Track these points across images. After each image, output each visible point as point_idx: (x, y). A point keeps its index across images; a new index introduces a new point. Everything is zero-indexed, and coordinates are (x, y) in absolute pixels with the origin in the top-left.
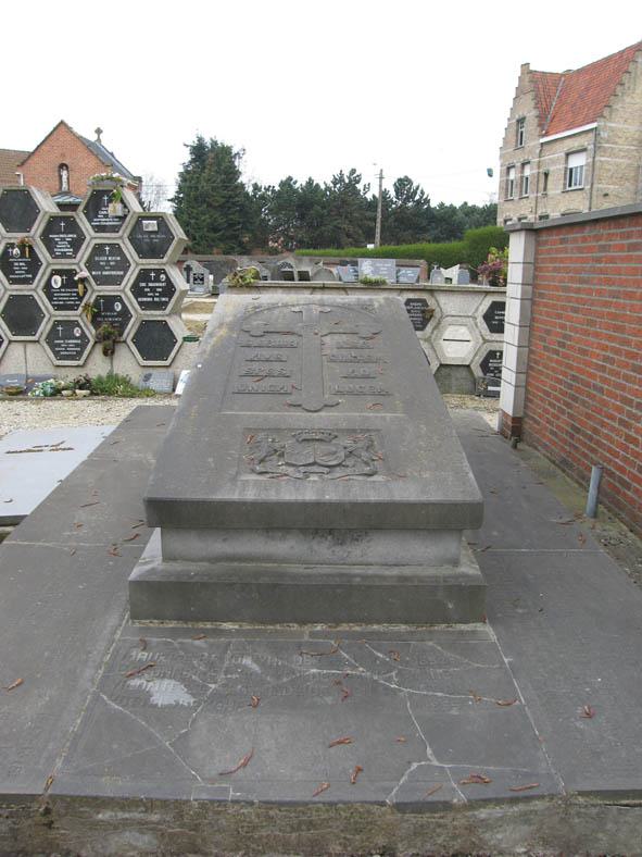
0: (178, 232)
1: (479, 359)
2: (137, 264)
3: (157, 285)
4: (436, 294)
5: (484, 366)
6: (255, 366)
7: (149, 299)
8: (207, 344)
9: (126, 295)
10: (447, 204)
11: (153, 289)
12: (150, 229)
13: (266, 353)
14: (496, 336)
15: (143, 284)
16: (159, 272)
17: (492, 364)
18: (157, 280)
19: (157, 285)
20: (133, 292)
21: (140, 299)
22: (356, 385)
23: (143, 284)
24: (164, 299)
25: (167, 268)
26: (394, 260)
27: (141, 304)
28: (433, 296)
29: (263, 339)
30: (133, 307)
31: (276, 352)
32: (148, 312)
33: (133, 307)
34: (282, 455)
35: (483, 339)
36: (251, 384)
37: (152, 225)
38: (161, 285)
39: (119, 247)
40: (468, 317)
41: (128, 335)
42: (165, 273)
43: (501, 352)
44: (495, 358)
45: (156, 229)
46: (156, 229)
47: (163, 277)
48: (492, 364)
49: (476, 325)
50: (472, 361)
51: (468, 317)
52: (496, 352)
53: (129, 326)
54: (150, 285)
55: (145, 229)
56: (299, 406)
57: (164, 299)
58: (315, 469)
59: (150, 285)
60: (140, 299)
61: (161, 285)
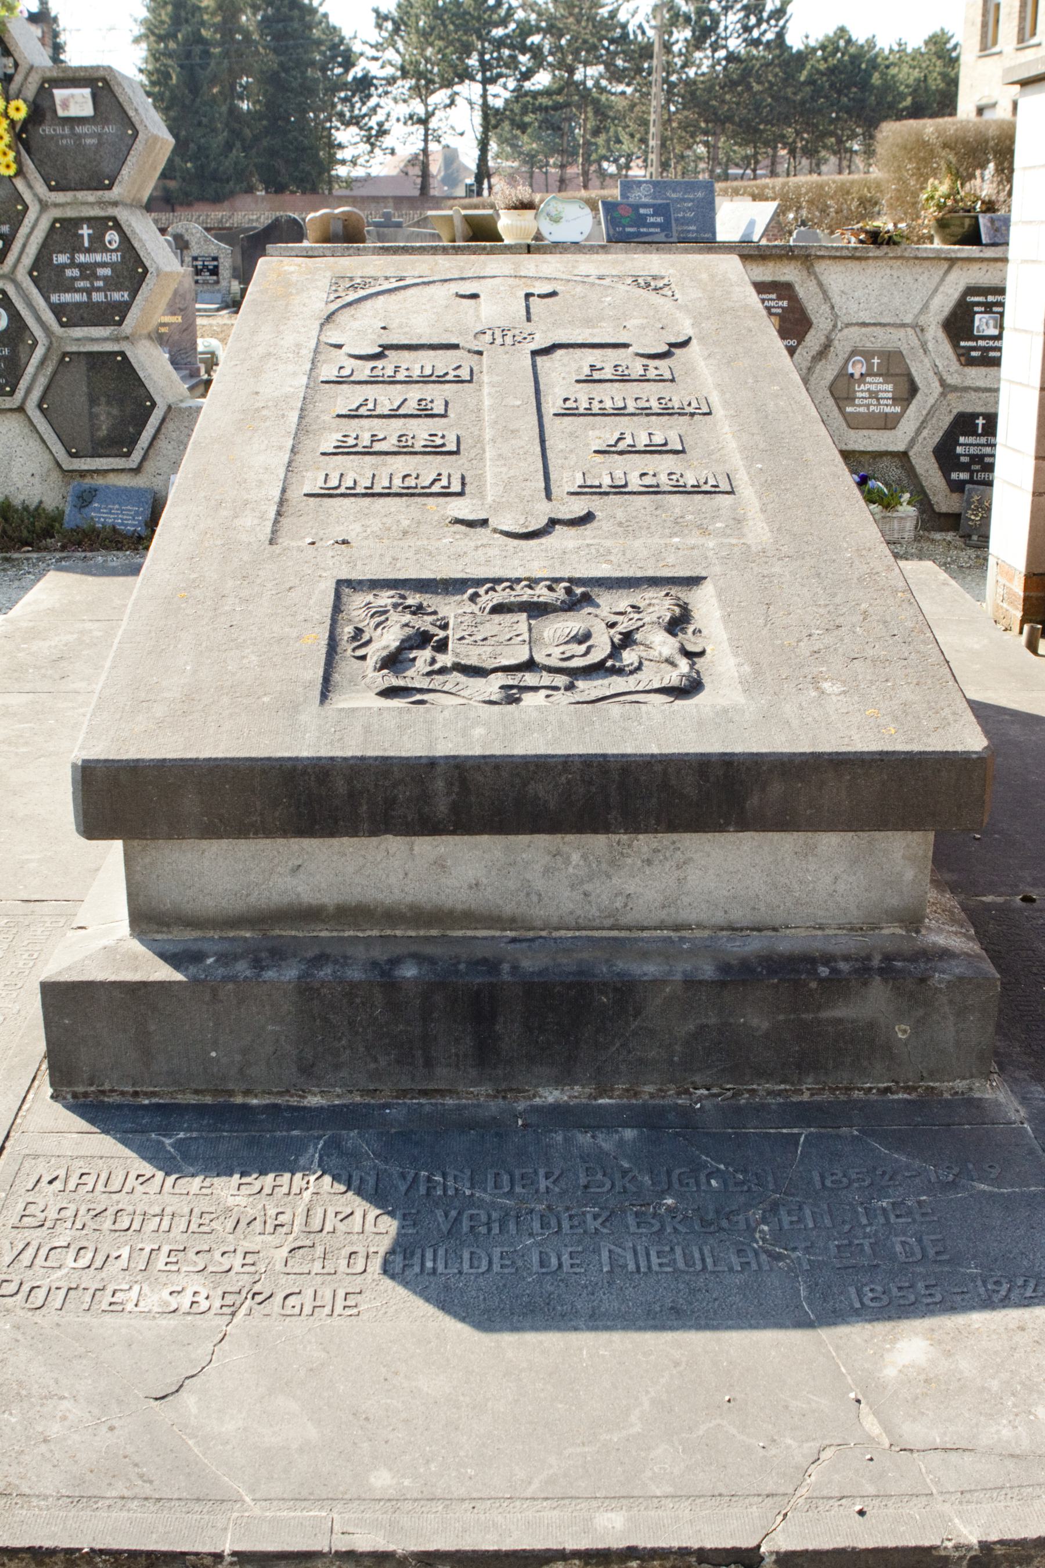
0: (155, 127)
1: (932, 436)
2: (44, 206)
3: (98, 257)
4: (820, 267)
5: (945, 453)
6: (363, 431)
7: (77, 297)
8: (217, 215)
9: (18, 285)
10: (859, 36)
11: (88, 271)
12: (74, 111)
13: (386, 398)
14: (976, 375)
15: (62, 259)
16: (102, 224)
17: (966, 446)
18: (98, 244)
19: (98, 257)
20: (35, 281)
21: (54, 298)
22: (630, 471)
23: (62, 259)
24: (116, 296)
25: (122, 215)
26: (718, 200)
27: (58, 310)
28: (810, 270)
29: (379, 364)
30: (39, 319)
31: (414, 394)
32: (78, 332)
33: (39, 319)
34: (442, 646)
35: (942, 383)
36: (357, 471)
37: (77, 102)
38: (106, 258)
39: (35, 266)
40: (903, 325)
41: (28, 391)
42: (118, 227)
43: (991, 420)
44: (974, 433)
45: (88, 111)
46: (88, 111)
47: (112, 237)
48: (966, 446)
49: (924, 345)
50: (913, 442)
51: (903, 325)
52: (975, 416)
53: (30, 370)
54: (81, 258)
55: (61, 113)
56: (484, 522)
57: (116, 296)
58: (530, 679)
59: (81, 258)
60: (54, 298)
61: (106, 258)
